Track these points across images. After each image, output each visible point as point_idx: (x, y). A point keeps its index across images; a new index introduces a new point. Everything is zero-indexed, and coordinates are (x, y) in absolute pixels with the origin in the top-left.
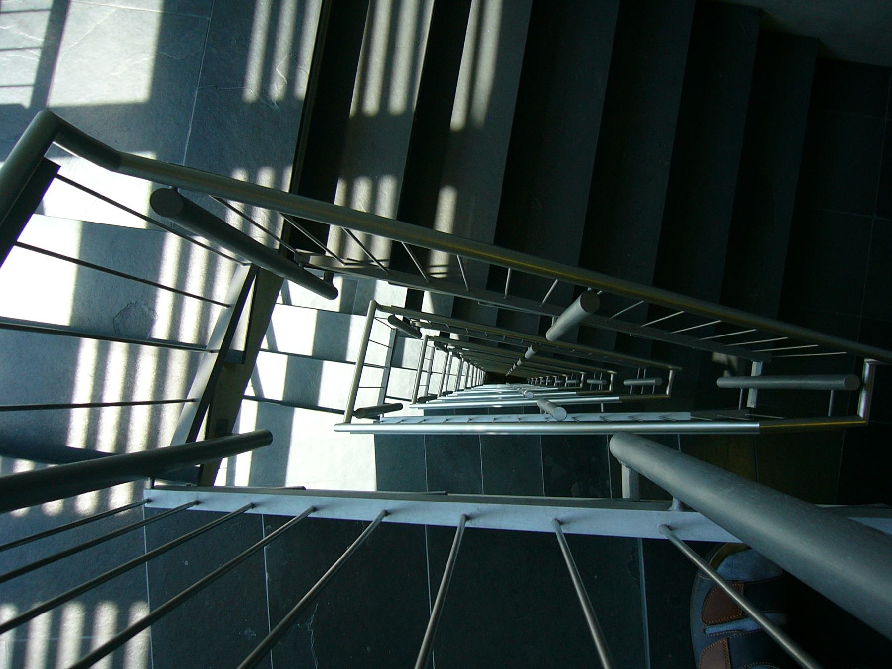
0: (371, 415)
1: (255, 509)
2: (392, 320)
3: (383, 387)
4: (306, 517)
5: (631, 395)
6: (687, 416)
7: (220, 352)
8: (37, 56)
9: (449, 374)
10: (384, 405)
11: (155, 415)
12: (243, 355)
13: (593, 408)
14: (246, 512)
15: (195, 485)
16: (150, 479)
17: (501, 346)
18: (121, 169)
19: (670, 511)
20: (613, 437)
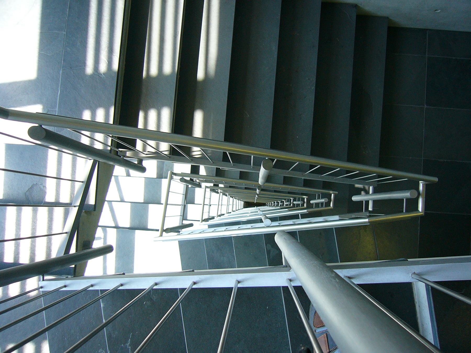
0: (175, 231)
1: (93, 287)
2: (182, 180)
3: (181, 216)
4: (152, 289)
5: (321, 207)
6: (337, 217)
7: (79, 206)
8: (105, 17)
9: (229, 205)
10: (183, 225)
11: (49, 242)
12: (94, 206)
13: (295, 217)
14: (118, 289)
15: (73, 277)
16: (42, 276)
17: (246, 188)
18: (9, 118)
19: (291, 271)
20: (276, 234)
